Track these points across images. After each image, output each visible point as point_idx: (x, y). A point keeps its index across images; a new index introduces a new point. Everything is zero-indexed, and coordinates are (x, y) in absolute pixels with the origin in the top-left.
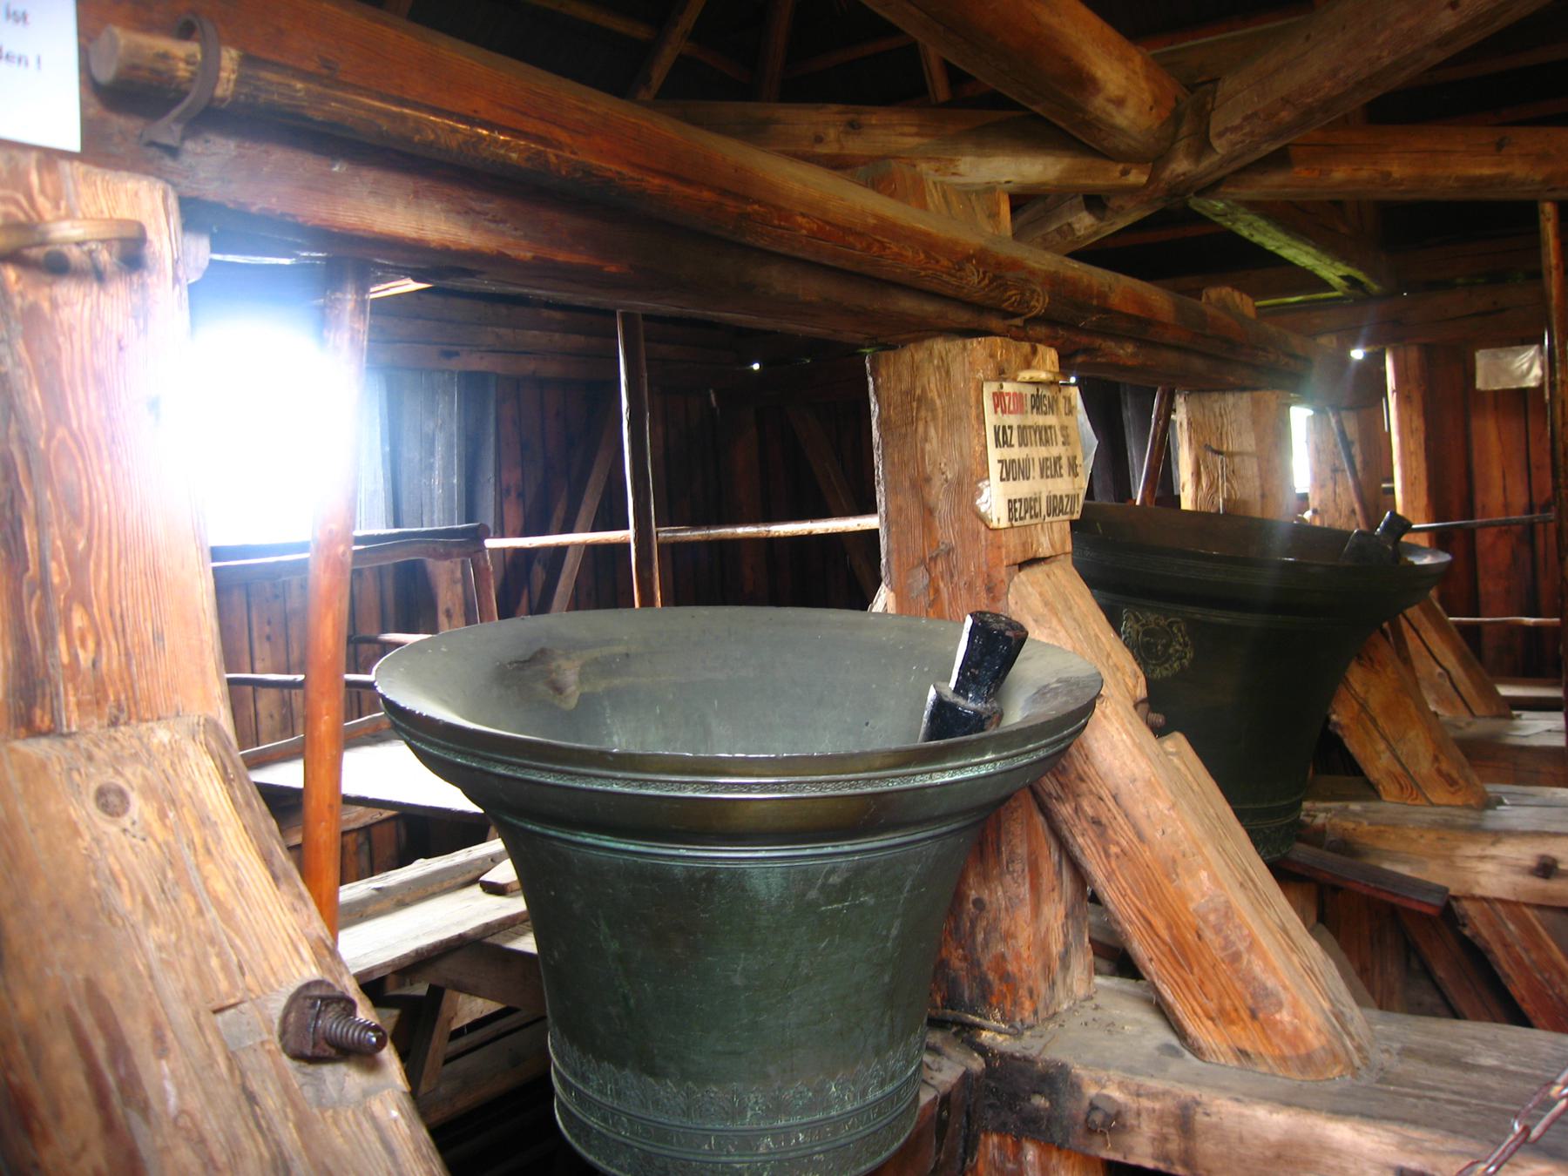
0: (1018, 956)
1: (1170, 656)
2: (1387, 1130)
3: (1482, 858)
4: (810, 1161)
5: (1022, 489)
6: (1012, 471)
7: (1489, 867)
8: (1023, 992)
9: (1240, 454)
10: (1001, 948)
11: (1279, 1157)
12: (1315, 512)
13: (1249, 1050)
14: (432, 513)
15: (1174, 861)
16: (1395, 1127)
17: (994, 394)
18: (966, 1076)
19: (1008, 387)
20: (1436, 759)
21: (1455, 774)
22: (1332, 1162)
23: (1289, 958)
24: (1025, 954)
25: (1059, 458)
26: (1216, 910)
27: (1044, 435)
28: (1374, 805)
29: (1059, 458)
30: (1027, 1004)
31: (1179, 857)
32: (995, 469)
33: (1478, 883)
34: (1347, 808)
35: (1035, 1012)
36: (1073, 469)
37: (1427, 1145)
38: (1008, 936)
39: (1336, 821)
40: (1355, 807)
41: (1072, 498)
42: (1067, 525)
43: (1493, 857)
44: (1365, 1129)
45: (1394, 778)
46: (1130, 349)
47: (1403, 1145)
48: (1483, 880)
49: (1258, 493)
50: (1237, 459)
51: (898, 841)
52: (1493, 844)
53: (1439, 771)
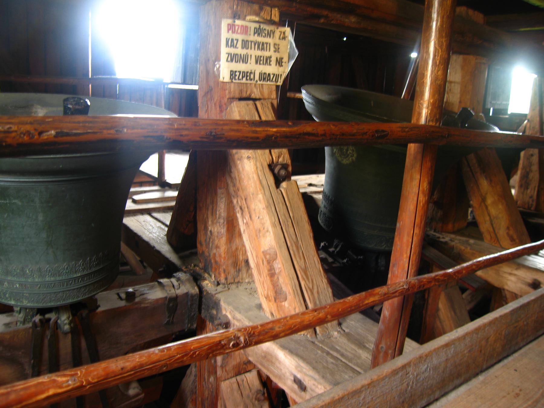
0: (220, 256)
1: (348, 155)
2: (294, 359)
3: (510, 274)
4: (23, 295)
5: (241, 67)
6: (232, 58)
7: (513, 278)
8: (221, 270)
9: (454, 82)
10: (215, 251)
11: (265, 357)
12: (528, 121)
13: (274, 314)
14: (196, 77)
15: (260, 231)
16: (297, 359)
17: (228, 25)
18: (187, 294)
19: (238, 22)
20: (508, 228)
21: (515, 237)
22: (278, 365)
23: (428, 298)
24: (223, 256)
25: (270, 57)
26: (270, 254)
27: (262, 46)
28: (479, 242)
29: (270, 57)
30: (223, 275)
31: (262, 229)
32: (224, 57)
33: (507, 284)
34: (467, 241)
35: (226, 279)
36: (279, 62)
37: (304, 370)
38: (217, 247)
39: (458, 245)
40: (472, 241)
41: (277, 76)
42: (274, 88)
43: (515, 275)
44: (288, 356)
45: (489, 233)
46: (353, 19)
47: (296, 367)
48: (509, 283)
49: (458, 101)
50: (453, 85)
51: (31, 180)
52: (517, 269)
53: (508, 234)
